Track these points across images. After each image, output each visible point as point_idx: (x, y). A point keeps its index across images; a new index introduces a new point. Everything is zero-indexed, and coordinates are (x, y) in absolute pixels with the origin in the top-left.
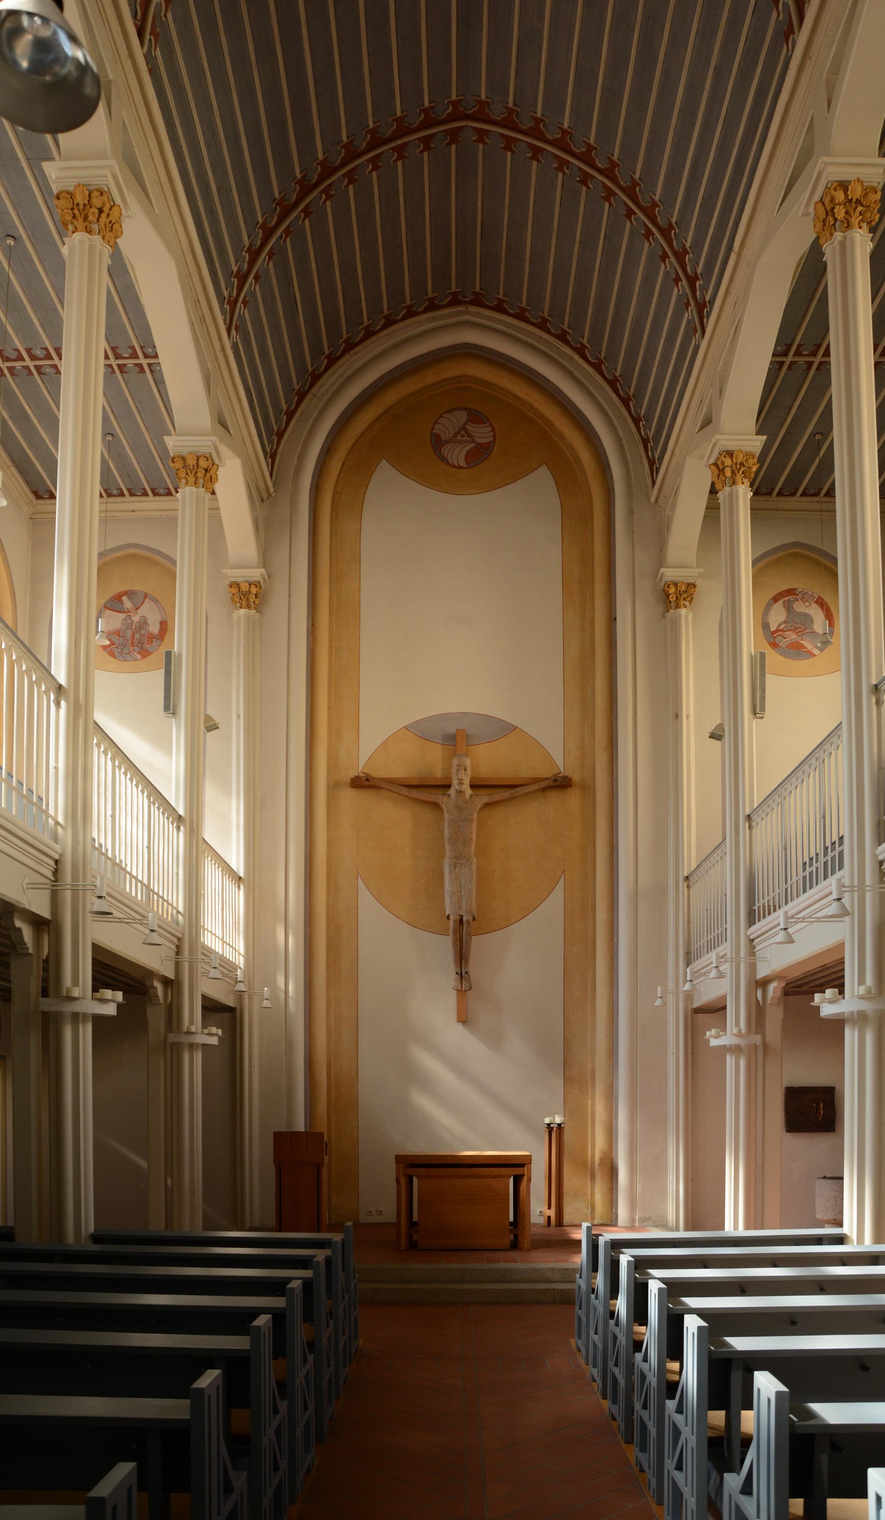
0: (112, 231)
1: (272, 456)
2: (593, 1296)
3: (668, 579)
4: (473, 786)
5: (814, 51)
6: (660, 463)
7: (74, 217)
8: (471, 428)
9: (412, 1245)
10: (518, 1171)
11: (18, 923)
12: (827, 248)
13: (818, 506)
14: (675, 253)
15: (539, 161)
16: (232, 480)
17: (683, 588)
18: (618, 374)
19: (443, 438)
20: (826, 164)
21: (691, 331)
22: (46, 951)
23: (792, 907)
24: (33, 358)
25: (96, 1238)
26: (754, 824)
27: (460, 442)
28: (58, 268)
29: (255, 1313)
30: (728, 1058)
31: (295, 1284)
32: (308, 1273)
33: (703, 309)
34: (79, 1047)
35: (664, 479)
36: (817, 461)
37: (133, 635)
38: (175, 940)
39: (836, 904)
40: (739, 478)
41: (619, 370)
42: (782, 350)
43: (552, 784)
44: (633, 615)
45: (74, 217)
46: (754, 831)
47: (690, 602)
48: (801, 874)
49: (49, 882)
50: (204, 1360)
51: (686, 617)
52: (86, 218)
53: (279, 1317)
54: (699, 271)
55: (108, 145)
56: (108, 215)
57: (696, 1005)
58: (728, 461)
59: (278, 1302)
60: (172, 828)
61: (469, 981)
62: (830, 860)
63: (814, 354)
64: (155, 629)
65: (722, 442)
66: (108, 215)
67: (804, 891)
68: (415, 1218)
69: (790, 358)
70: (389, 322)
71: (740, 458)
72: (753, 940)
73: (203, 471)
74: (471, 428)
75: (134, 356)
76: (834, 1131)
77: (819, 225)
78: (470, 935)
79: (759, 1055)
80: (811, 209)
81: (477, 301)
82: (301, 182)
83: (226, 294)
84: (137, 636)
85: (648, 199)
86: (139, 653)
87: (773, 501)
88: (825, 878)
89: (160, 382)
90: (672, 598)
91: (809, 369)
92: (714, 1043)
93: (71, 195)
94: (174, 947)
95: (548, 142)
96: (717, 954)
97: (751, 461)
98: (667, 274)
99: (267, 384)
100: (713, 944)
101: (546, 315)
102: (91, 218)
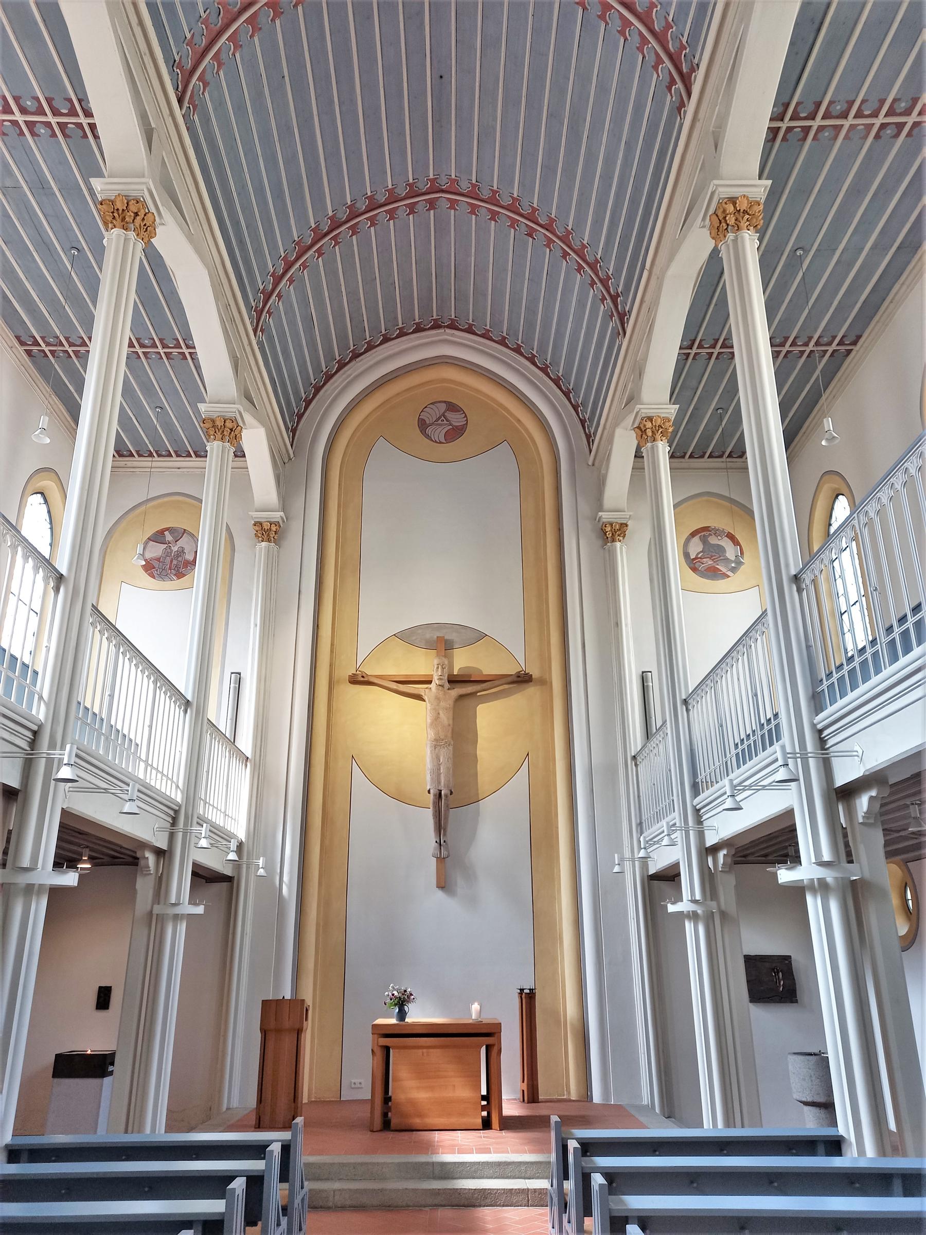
0: (147, 230)
3: (604, 520)
4: (449, 682)
5: (701, 115)
7: (114, 218)
8: (449, 415)
9: (386, 1125)
12: (723, 254)
13: (723, 465)
14: (601, 280)
15: (496, 221)
16: (256, 440)
18: (560, 375)
19: (428, 422)
20: (717, 186)
23: (737, 775)
26: (690, 707)
28: (99, 251)
30: (687, 924)
31: (276, 1148)
33: (623, 318)
36: (720, 430)
37: (172, 561)
38: (172, 813)
39: (782, 769)
40: (658, 436)
42: (688, 344)
43: (516, 679)
44: (578, 549)
45: (114, 218)
46: (691, 713)
47: (624, 537)
48: (733, 752)
51: (621, 549)
52: (123, 219)
53: (255, 1182)
54: (620, 290)
55: (146, 169)
56: (143, 219)
57: (652, 871)
58: (649, 425)
59: (256, 1165)
60: (178, 712)
61: (447, 849)
62: (770, 733)
63: (713, 346)
65: (643, 411)
66: (143, 219)
67: (739, 767)
71: (659, 422)
72: (699, 810)
73: (228, 430)
74: (448, 414)
75: (178, 346)
76: (796, 1002)
77: (714, 231)
78: (448, 807)
79: (716, 921)
80: (707, 222)
81: (453, 326)
83: (253, 304)
84: (175, 562)
85: (579, 243)
86: (175, 575)
88: (771, 744)
89: (198, 368)
90: (609, 535)
91: (710, 358)
92: (671, 908)
94: (170, 820)
95: (502, 207)
96: (668, 823)
97: (667, 424)
98: (595, 296)
99: (289, 377)
100: (658, 817)
101: (505, 334)
102: (127, 219)
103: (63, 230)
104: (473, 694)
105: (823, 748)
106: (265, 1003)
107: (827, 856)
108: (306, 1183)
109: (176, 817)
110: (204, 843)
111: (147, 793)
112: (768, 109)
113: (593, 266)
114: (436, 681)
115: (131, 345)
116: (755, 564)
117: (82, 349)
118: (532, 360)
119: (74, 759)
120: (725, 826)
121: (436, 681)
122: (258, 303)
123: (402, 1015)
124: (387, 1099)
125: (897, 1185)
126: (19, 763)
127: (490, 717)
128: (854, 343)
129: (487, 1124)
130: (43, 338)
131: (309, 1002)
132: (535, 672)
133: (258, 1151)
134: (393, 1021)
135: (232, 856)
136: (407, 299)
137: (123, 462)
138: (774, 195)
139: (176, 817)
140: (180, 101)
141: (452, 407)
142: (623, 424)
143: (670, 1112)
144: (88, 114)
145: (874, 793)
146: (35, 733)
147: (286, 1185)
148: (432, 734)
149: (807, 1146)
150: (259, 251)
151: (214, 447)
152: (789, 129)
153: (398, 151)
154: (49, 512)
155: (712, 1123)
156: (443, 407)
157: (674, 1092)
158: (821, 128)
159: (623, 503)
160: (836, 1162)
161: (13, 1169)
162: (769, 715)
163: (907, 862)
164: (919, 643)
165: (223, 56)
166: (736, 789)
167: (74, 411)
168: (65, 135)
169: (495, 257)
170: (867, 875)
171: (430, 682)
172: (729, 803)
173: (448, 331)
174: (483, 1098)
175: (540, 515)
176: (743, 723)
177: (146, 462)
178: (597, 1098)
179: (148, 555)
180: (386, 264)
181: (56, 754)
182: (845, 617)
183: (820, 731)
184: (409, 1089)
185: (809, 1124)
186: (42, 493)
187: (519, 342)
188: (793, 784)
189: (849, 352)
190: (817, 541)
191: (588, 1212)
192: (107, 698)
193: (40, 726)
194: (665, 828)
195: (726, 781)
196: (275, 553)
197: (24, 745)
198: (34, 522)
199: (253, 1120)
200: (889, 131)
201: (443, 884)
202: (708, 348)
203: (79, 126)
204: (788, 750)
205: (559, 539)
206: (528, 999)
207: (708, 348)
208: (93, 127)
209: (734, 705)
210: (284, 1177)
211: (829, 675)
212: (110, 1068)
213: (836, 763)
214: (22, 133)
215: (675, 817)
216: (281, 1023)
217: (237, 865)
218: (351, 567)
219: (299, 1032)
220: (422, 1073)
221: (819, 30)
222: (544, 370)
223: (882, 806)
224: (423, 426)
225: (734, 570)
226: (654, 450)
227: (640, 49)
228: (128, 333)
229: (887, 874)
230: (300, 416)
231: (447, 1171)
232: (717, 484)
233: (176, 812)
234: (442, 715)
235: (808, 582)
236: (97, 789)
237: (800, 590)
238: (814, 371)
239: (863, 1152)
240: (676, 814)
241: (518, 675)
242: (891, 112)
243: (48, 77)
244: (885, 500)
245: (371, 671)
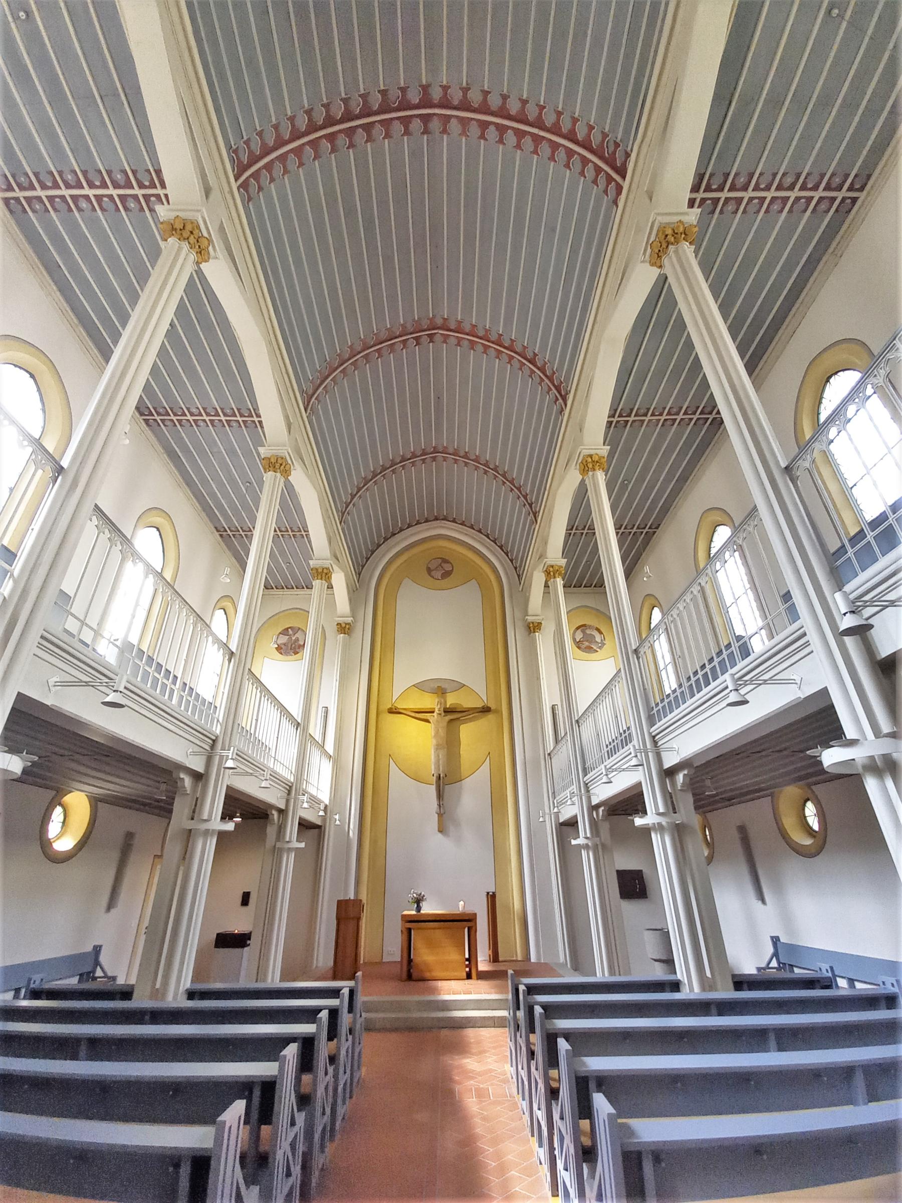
0: (286, 473)
4: (445, 712)
9: (410, 977)
10: (469, 924)
11: (182, 776)
12: (587, 482)
16: (339, 580)
21: (532, 523)
23: (609, 763)
25: (191, 995)
28: (261, 483)
31: (346, 991)
33: (535, 515)
42: (570, 528)
48: (606, 750)
53: (334, 1013)
57: (561, 821)
60: (293, 730)
63: (584, 529)
69: (574, 531)
73: (324, 574)
79: (600, 850)
81: (445, 519)
82: (373, 472)
87: (572, 589)
89: (310, 542)
92: (574, 842)
93: (269, 459)
100: (564, 788)
103: (243, 474)
104: (458, 719)
105: (588, 791)
106: (339, 902)
107: (661, 810)
108: (363, 1014)
109: (290, 790)
110: (305, 805)
111: (275, 777)
112: (606, 412)
113: (519, 489)
114: (437, 711)
115: (275, 531)
116: (612, 645)
117: (249, 533)
118: (487, 536)
119: (235, 756)
120: (603, 792)
121: (437, 711)
122: (343, 508)
123: (419, 909)
124: (410, 961)
125: (714, 1009)
126: (204, 758)
127: (467, 732)
128: (657, 528)
129: (469, 976)
131: (364, 901)
132: (493, 706)
133: (335, 993)
134: (414, 912)
135: (322, 813)
136: (421, 507)
137: (267, 592)
138: (611, 454)
139: (290, 790)
140: (306, 410)
141: (445, 561)
143: (576, 967)
144: (258, 416)
145: (686, 772)
146: (214, 741)
147: (351, 1015)
148: (434, 742)
149: (659, 986)
150: (344, 483)
151: (317, 583)
152: (618, 422)
153: (417, 433)
155: (602, 974)
156: (440, 561)
157: (579, 955)
158: (634, 421)
159: (539, 612)
160: (677, 996)
161: (191, 1004)
162: (625, 728)
163: (705, 813)
165: (329, 388)
166: (609, 770)
167: (243, 565)
168: (246, 427)
169: (470, 488)
170: (685, 821)
172: (605, 779)
174: (467, 960)
175: (494, 619)
176: (610, 734)
177: (280, 592)
178: (533, 959)
179: (279, 642)
180: (410, 489)
181: (224, 753)
183: (654, 737)
184: (424, 955)
185: (658, 973)
188: (640, 767)
190: (646, 633)
191: (532, 1030)
193: (217, 737)
195: (603, 766)
197: (207, 748)
198: (218, 622)
199: (331, 973)
200: (669, 423)
201: (441, 831)
202: (581, 531)
203: (254, 422)
204: (637, 747)
205: (503, 634)
206: (492, 898)
207: (581, 531)
208: (260, 422)
209: (603, 724)
210: (351, 1009)
211: (657, 705)
212: (248, 942)
213: (664, 755)
214: (224, 426)
215: (574, 788)
216: (348, 914)
217: (324, 818)
218: (389, 646)
219: (359, 919)
220: (431, 945)
221: (630, 375)
223: (691, 779)
224: (429, 570)
225: (600, 648)
226: (555, 583)
227: (540, 384)
228: (274, 525)
229: (695, 820)
230: (363, 566)
231: (446, 1006)
232: (590, 602)
233: (290, 787)
235: (642, 653)
236: (247, 774)
237: (638, 658)
238: (638, 540)
239: (692, 990)
241: (483, 708)
242: (669, 414)
243: (238, 398)
244: (681, 608)
245: (400, 705)
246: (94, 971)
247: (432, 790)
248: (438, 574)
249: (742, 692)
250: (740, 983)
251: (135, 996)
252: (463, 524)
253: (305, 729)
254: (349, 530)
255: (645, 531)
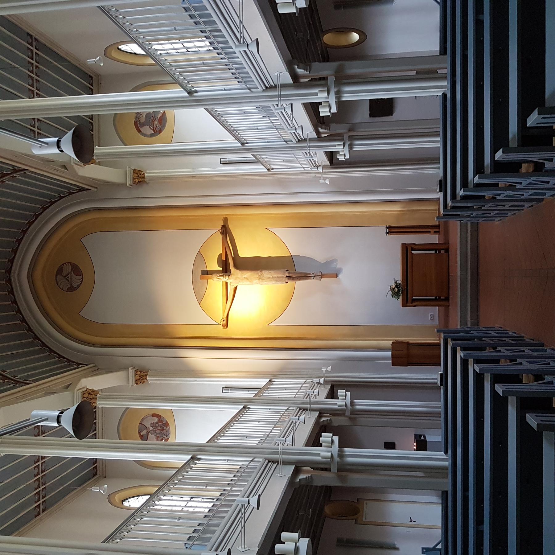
1: (79, 365)
2: (518, 186)
6: (80, 187)
10: (409, 249)
17: (136, 175)
22: (309, 468)
24: (38, 474)
25: (446, 452)
27: (71, 279)
29: (494, 392)
30: (354, 149)
32: (471, 361)
33: (16, 170)
34: (354, 455)
35: (86, 185)
38: (301, 411)
41: (38, 206)
47: (142, 172)
49: (278, 466)
50: (522, 422)
51: (148, 173)
53: (497, 378)
57: (328, 163)
60: (250, 411)
64: (156, 419)
68: (434, 298)
70: (19, 311)
72: (299, 140)
78: (295, 273)
84: (159, 428)
86: (167, 427)
90: (140, 180)
104: (234, 259)
105: (275, 86)
128: (31, 36)
130: (36, 502)
141: (60, 271)
142: (77, 170)
154: (132, 497)
163: (322, 31)
164: (203, 3)
171: (227, 283)
172: (254, 49)
173: (12, 274)
182: (189, 50)
183: (266, 87)
186: (123, 501)
187: (20, 231)
189: (36, 39)
192: (248, 439)
194: (242, 49)
196: (153, 372)
216: (404, 355)
222: (37, 216)
224: (72, 289)
230: (69, 361)
234: (245, 276)
237: (247, 143)
240: (270, 104)
241: (222, 233)
245: (221, 316)
246: (439, 550)
247: (300, 284)
248: (76, 280)
249: (249, 41)
250: (443, 51)
251: (446, 489)
252: (15, 251)
253: (250, 401)
254: (32, 376)
255: (35, 50)
